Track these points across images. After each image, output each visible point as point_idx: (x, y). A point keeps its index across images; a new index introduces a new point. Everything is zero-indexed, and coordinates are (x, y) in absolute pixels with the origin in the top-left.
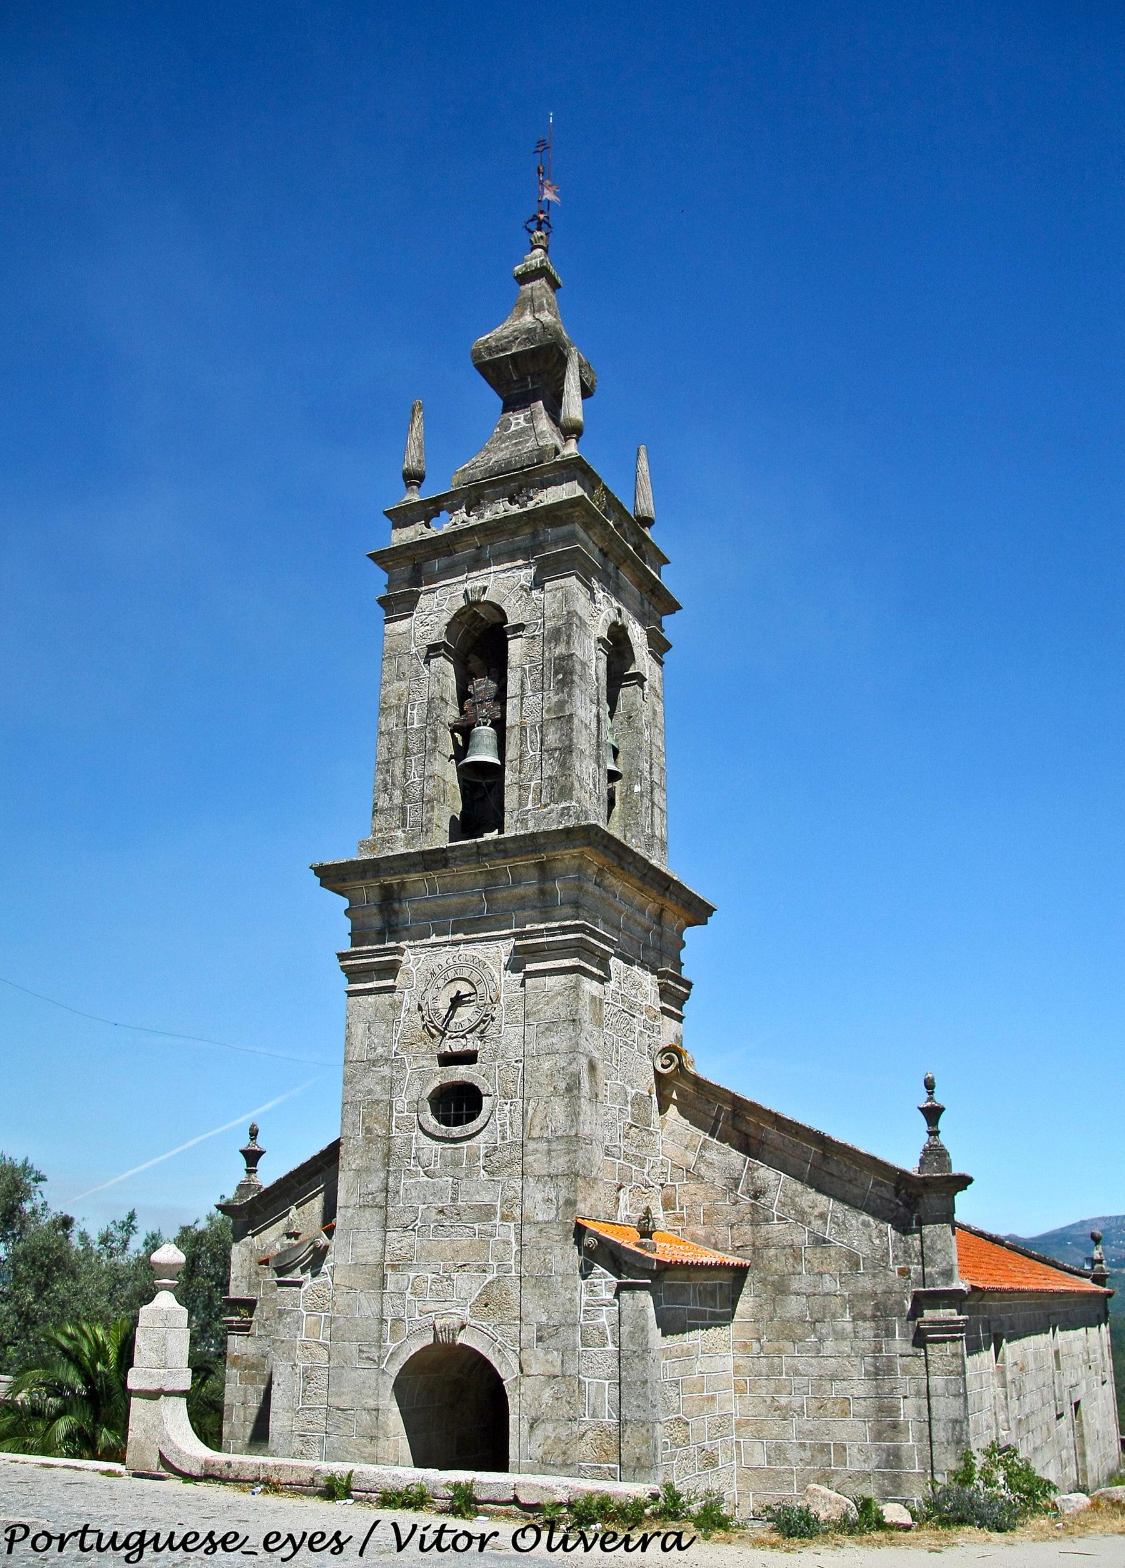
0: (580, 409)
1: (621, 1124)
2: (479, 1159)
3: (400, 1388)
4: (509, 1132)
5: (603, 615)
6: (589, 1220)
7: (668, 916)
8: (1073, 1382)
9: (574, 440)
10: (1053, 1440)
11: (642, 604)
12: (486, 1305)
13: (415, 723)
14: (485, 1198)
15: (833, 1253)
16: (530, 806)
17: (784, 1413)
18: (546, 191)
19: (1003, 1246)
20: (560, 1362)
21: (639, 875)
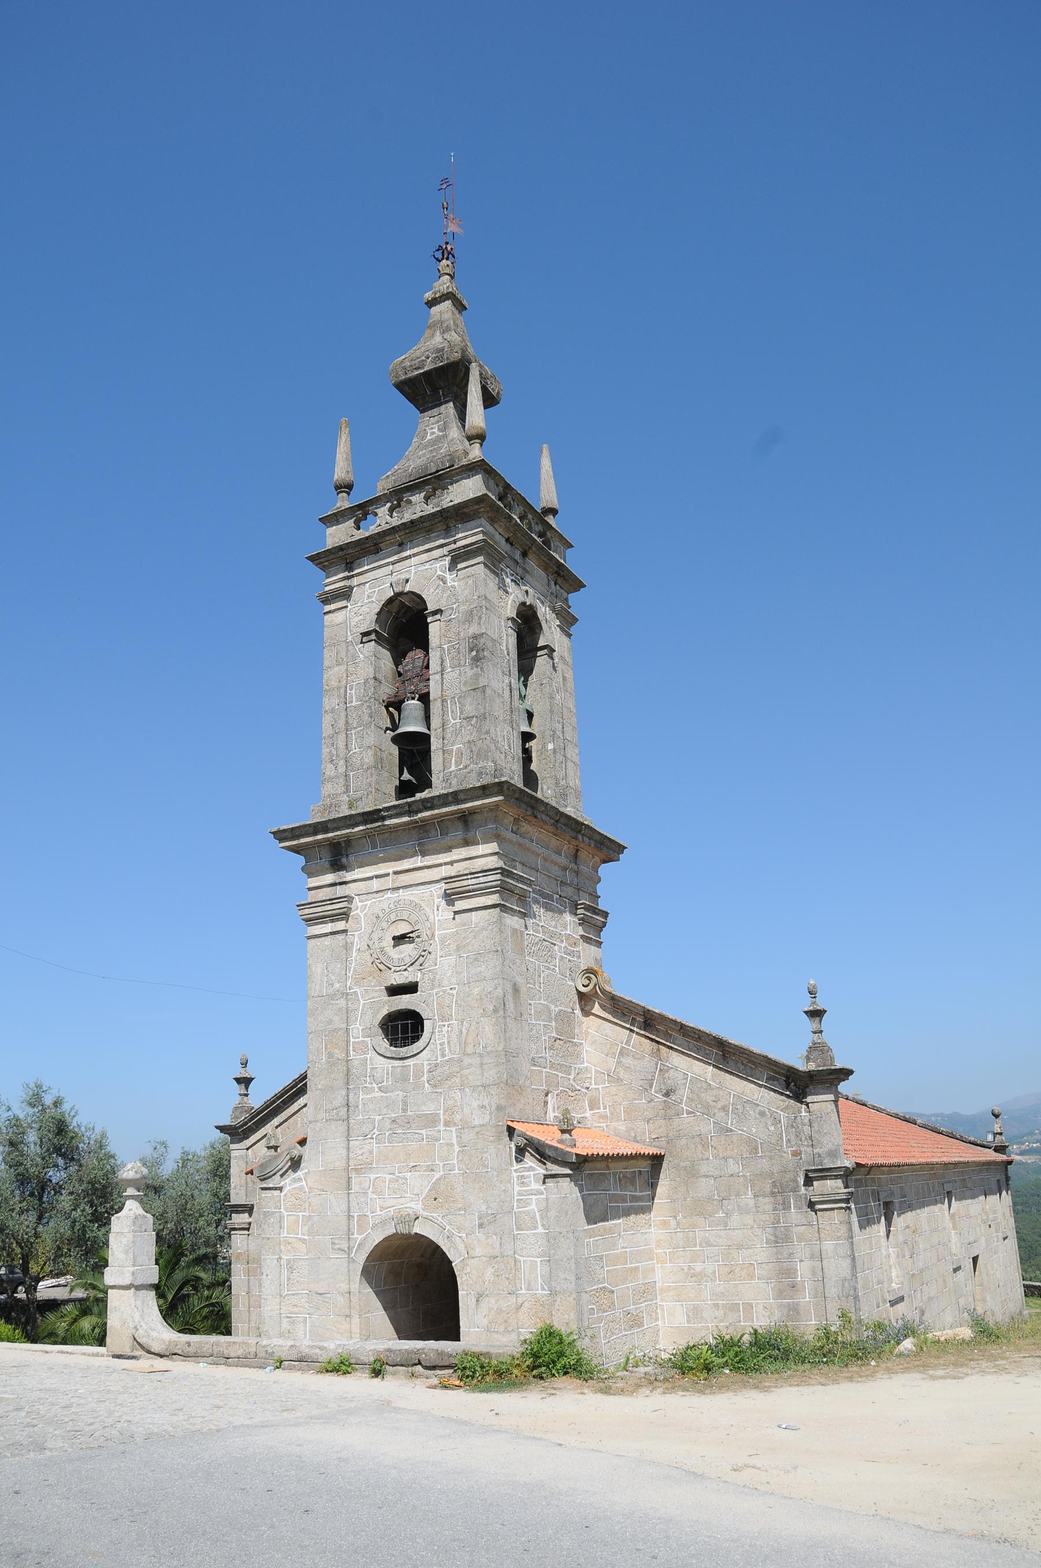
0: (482, 417)
1: (546, 1038)
2: (424, 1075)
3: (368, 1273)
4: (447, 1051)
5: (512, 597)
6: (518, 1122)
7: (583, 855)
8: (972, 1239)
9: (478, 445)
10: (949, 1289)
11: (549, 584)
12: (435, 1199)
13: (354, 701)
14: (429, 1108)
15: (735, 1139)
16: (453, 768)
17: (699, 1277)
18: (450, 224)
19: (915, 1124)
20: (498, 1245)
21: (552, 821)
